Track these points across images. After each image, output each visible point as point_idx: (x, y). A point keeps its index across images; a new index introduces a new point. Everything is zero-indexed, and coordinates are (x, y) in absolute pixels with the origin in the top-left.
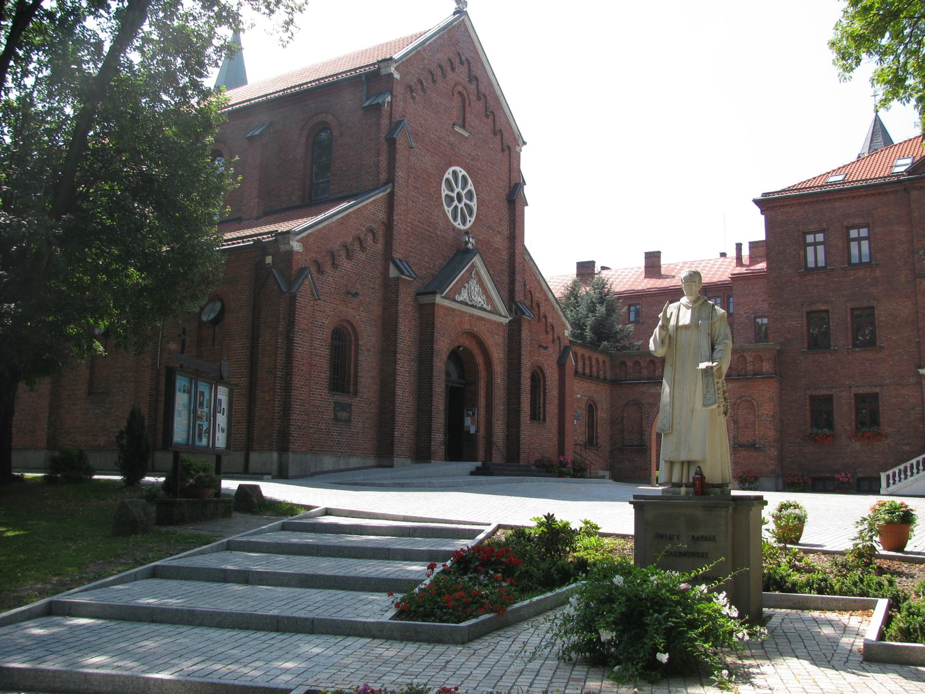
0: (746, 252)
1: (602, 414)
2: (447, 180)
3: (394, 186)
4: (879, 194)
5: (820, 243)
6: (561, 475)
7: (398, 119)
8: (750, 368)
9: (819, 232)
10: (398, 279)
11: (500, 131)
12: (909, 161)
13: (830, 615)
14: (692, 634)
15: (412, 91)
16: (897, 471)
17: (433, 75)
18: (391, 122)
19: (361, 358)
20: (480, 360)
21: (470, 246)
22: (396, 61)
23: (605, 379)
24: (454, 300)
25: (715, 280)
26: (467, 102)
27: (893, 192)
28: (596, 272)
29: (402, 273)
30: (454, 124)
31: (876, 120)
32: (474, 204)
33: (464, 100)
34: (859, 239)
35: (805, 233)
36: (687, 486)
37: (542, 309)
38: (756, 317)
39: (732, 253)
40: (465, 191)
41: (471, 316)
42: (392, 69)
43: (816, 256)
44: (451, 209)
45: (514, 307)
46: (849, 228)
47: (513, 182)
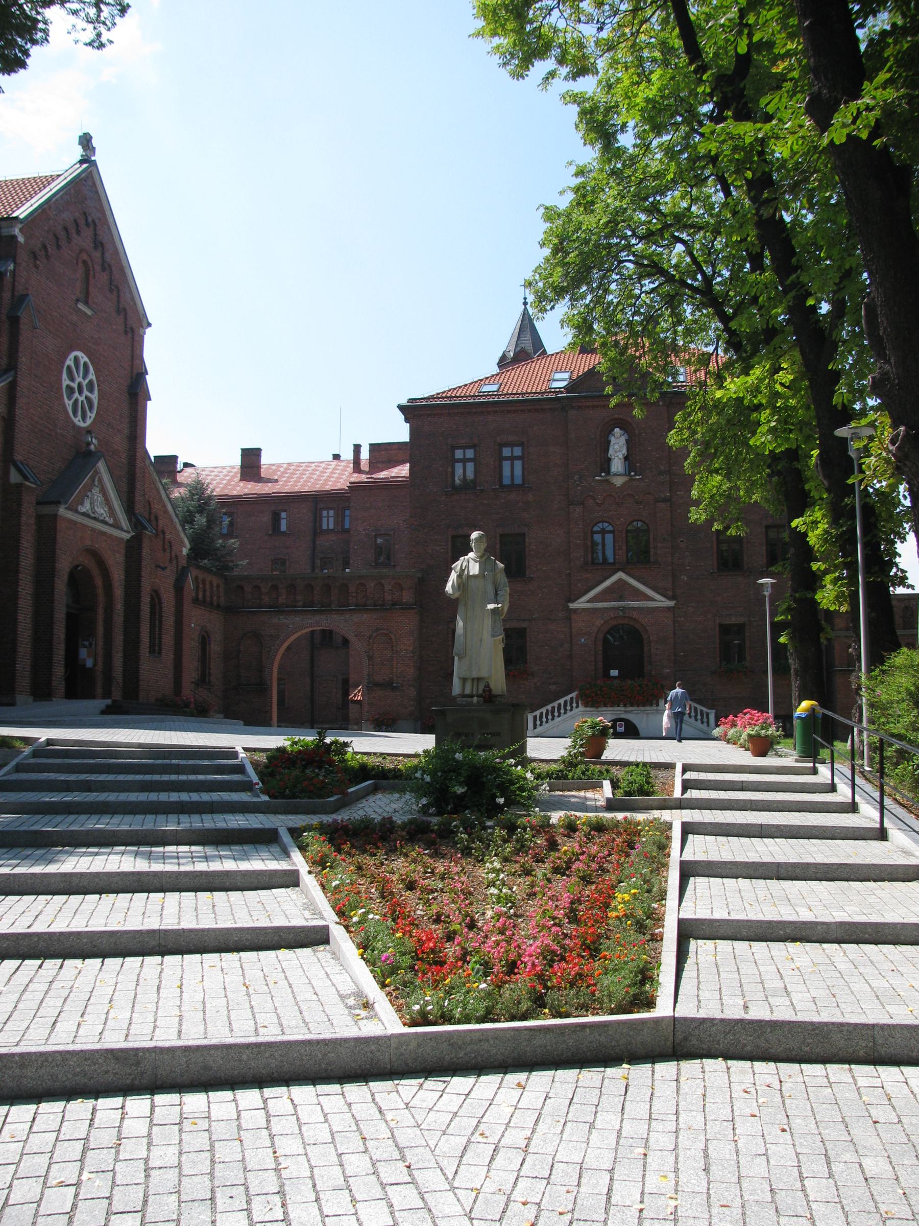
0: (365, 455)
1: (215, 648)
2: (69, 368)
3: (16, 373)
4: (536, 410)
5: (469, 460)
6: (185, 714)
8: (388, 597)
10: (19, 486)
11: (125, 309)
12: (566, 376)
14: (512, 788)
16: (544, 712)
17: (57, 239)
18: (13, 296)
20: (99, 582)
21: (92, 447)
23: (218, 606)
24: (77, 511)
25: (328, 488)
26: (92, 273)
27: (551, 409)
28: (179, 469)
29: (26, 478)
30: (78, 300)
31: (524, 314)
32: (95, 397)
33: (87, 271)
34: (512, 459)
35: (454, 448)
36: (478, 696)
37: (161, 523)
39: (348, 455)
40: (87, 381)
41: (93, 530)
42: (17, 231)
43: (463, 472)
44: (71, 402)
45: (134, 520)
47: (135, 372)
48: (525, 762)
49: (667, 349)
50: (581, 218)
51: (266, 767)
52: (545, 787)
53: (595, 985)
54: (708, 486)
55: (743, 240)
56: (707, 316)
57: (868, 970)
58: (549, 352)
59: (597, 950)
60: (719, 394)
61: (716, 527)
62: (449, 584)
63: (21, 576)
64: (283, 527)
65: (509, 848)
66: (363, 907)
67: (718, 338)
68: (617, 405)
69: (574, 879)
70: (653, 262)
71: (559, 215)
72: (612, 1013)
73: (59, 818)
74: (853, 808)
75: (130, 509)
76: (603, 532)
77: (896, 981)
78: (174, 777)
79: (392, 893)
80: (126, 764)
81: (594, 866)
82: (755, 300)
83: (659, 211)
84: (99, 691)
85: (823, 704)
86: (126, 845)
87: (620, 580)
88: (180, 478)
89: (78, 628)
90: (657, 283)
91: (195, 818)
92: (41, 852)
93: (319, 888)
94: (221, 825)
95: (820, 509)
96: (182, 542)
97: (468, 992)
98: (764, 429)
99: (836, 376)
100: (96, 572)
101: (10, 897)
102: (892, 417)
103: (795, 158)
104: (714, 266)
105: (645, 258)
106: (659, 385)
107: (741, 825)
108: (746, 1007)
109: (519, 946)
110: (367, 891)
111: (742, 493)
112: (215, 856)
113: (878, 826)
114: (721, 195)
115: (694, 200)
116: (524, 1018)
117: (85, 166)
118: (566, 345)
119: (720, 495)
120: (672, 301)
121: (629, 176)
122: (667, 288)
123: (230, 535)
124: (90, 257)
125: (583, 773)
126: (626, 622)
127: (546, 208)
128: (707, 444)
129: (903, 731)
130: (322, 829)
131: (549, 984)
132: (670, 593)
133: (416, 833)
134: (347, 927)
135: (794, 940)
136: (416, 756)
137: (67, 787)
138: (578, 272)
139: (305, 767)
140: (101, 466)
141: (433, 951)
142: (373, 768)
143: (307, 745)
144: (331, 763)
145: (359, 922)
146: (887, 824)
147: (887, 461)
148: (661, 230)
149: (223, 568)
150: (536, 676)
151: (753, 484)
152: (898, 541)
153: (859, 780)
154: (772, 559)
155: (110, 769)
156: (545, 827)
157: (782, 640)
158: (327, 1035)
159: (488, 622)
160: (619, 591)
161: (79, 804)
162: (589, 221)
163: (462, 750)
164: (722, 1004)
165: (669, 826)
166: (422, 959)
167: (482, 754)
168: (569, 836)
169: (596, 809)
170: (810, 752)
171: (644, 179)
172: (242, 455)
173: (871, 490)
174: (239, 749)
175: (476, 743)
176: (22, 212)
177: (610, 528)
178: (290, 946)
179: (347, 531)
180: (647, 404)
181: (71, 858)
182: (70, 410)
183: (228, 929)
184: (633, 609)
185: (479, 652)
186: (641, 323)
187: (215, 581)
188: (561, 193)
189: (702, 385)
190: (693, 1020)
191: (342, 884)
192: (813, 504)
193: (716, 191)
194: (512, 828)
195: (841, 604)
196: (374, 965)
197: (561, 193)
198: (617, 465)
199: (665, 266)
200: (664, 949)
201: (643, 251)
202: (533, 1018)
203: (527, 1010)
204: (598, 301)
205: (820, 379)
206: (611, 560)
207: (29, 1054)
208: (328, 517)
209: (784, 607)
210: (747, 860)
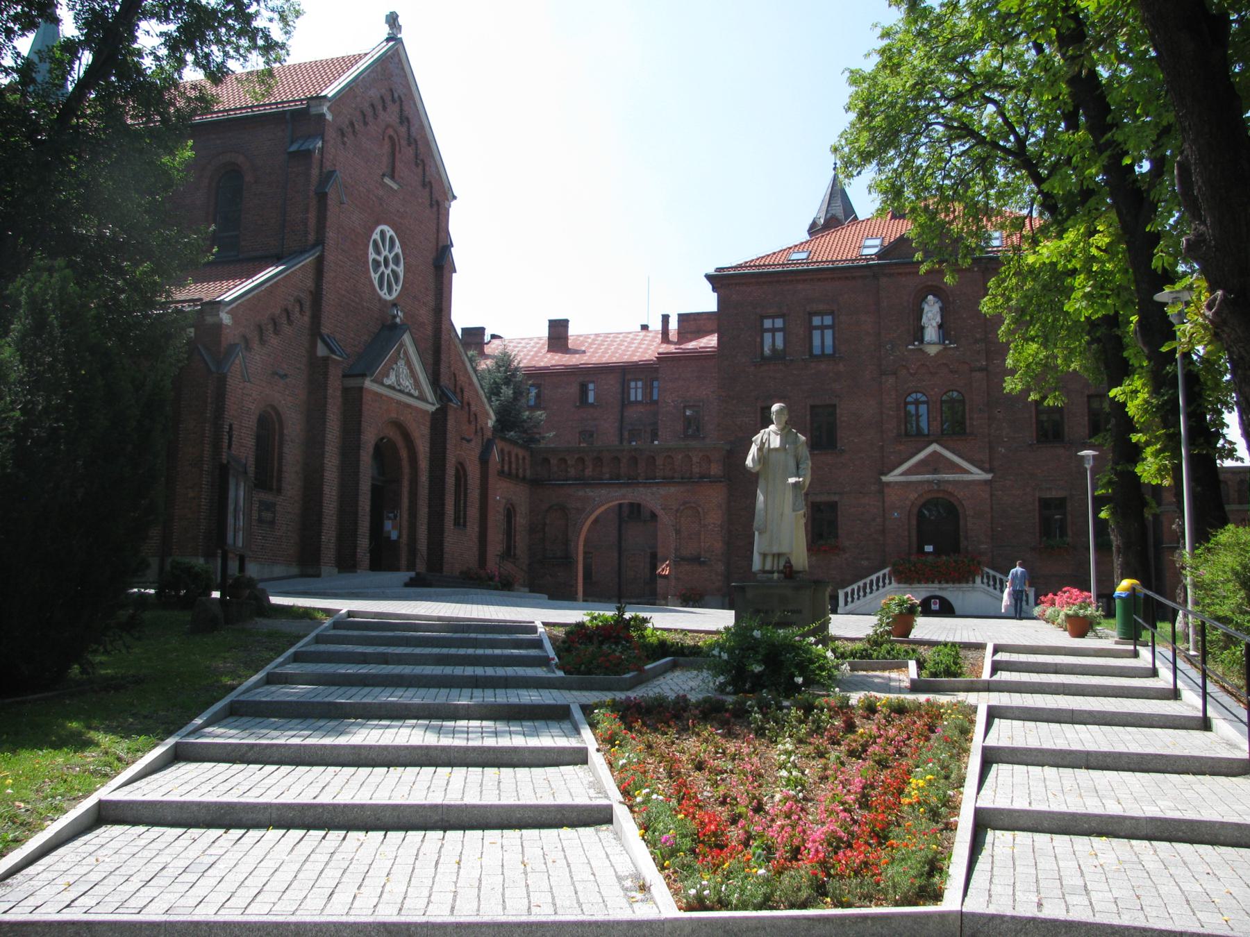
0: (673, 325)
1: (521, 520)
2: (375, 242)
4: (847, 278)
5: (779, 330)
6: (489, 587)
7: (329, 168)
8: (696, 470)
9: (778, 317)
10: (326, 359)
11: (430, 183)
12: (877, 242)
13: (878, 673)
14: (812, 667)
15: (343, 135)
17: (364, 116)
19: (286, 450)
20: (404, 454)
21: (398, 320)
22: (330, 100)
23: (524, 479)
24: (382, 384)
25: (635, 359)
30: (384, 175)
32: (400, 270)
33: (393, 146)
34: (822, 328)
35: (763, 317)
36: (779, 572)
38: (685, 407)
39: (656, 325)
41: (399, 402)
42: (325, 109)
43: (772, 342)
44: (377, 276)
46: (812, 314)
47: (441, 244)
48: (826, 640)
49: (978, 212)
50: (887, 81)
51: (564, 642)
52: (846, 667)
53: (880, 874)
54: (1023, 355)
55: (1055, 99)
56: (1020, 178)
57: (1180, 872)
58: (861, 218)
59: (886, 838)
60: (1031, 259)
61: (1033, 397)
62: (749, 458)
63: (327, 448)
64: (591, 399)
65: (804, 729)
66: (648, 787)
67: (1033, 200)
68: (928, 272)
69: (870, 763)
70: (963, 123)
71: (864, 79)
72: (897, 904)
73: (354, 690)
74: (1175, 694)
75: (435, 382)
76: (917, 403)
77: (1211, 885)
78: (470, 651)
79: (679, 773)
80: (423, 637)
81: (891, 749)
82: (1069, 161)
83: (968, 71)
84: (404, 562)
85: (1146, 583)
86: (418, 718)
87: (935, 452)
88: (488, 350)
89: (383, 499)
90: (967, 146)
91: (489, 692)
92: (333, 723)
93: (606, 767)
94: (514, 700)
95: (1140, 378)
96: (488, 414)
97: (746, 877)
98: (1078, 294)
99: (1156, 238)
100: (400, 443)
101: (300, 768)
102: (1208, 280)
103: (1101, 13)
104: (1027, 125)
105: (955, 120)
106: (970, 250)
107: (1051, 710)
108: (1040, 905)
109: (804, 832)
110: (656, 771)
111: (1059, 361)
112: (504, 732)
113: (1200, 714)
114: (1033, 52)
115: (1005, 59)
116: (803, 906)
117: (391, 43)
118: (873, 210)
119: (1037, 364)
120: (984, 164)
121: (937, 37)
122: (978, 150)
123: (537, 407)
124: (396, 131)
125: (888, 653)
126: (941, 495)
127: (852, 72)
128: (1021, 311)
129: (1229, 614)
130: (614, 706)
131: (832, 871)
132: (987, 466)
133: (711, 712)
134: (631, 808)
135: (1100, 834)
136: (717, 632)
137: (364, 659)
138: (885, 136)
139: (602, 643)
140: (407, 338)
141: (715, 834)
142: (673, 645)
143: (606, 620)
144: (629, 638)
145: (643, 802)
146: (1210, 713)
147: (1204, 327)
148: (970, 91)
149: (530, 441)
150: (841, 550)
151: (1072, 351)
152: (1225, 411)
153: (1181, 664)
154: (1095, 429)
155: (408, 642)
156: (844, 708)
157: (1103, 515)
158: (600, 917)
159: (789, 496)
160: (934, 463)
161: (375, 676)
162: (895, 84)
163: (760, 627)
164: (1014, 901)
165: (974, 709)
166: (703, 842)
167: (781, 631)
168: (868, 718)
169: (900, 690)
170: (1132, 634)
171: (952, 38)
173: (1195, 357)
174: (538, 624)
175: (776, 619)
176: (330, 91)
177: (924, 399)
178: (573, 825)
179: (656, 402)
180: (958, 270)
181: (363, 731)
182: (376, 283)
183: (511, 806)
184: (948, 482)
185: (781, 529)
186: (951, 187)
187: (521, 453)
188: (867, 56)
189: (1017, 249)
190: (982, 915)
191: (630, 763)
192: (1133, 373)
193: (1029, 48)
194: (808, 708)
195: (1163, 478)
196: (654, 846)
197: (867, 56)
198: (931, 334)
199: (976, 128)
200: (957, 839)
201: (953, 112)
202: (813, 907)
203: (807, 899)
204: (907, 165)
205: (1138, 241)
206: (926, 432)
207: (304, 923)
208: (636, 388)
209: (1105, 480)
210: (1054, 747)
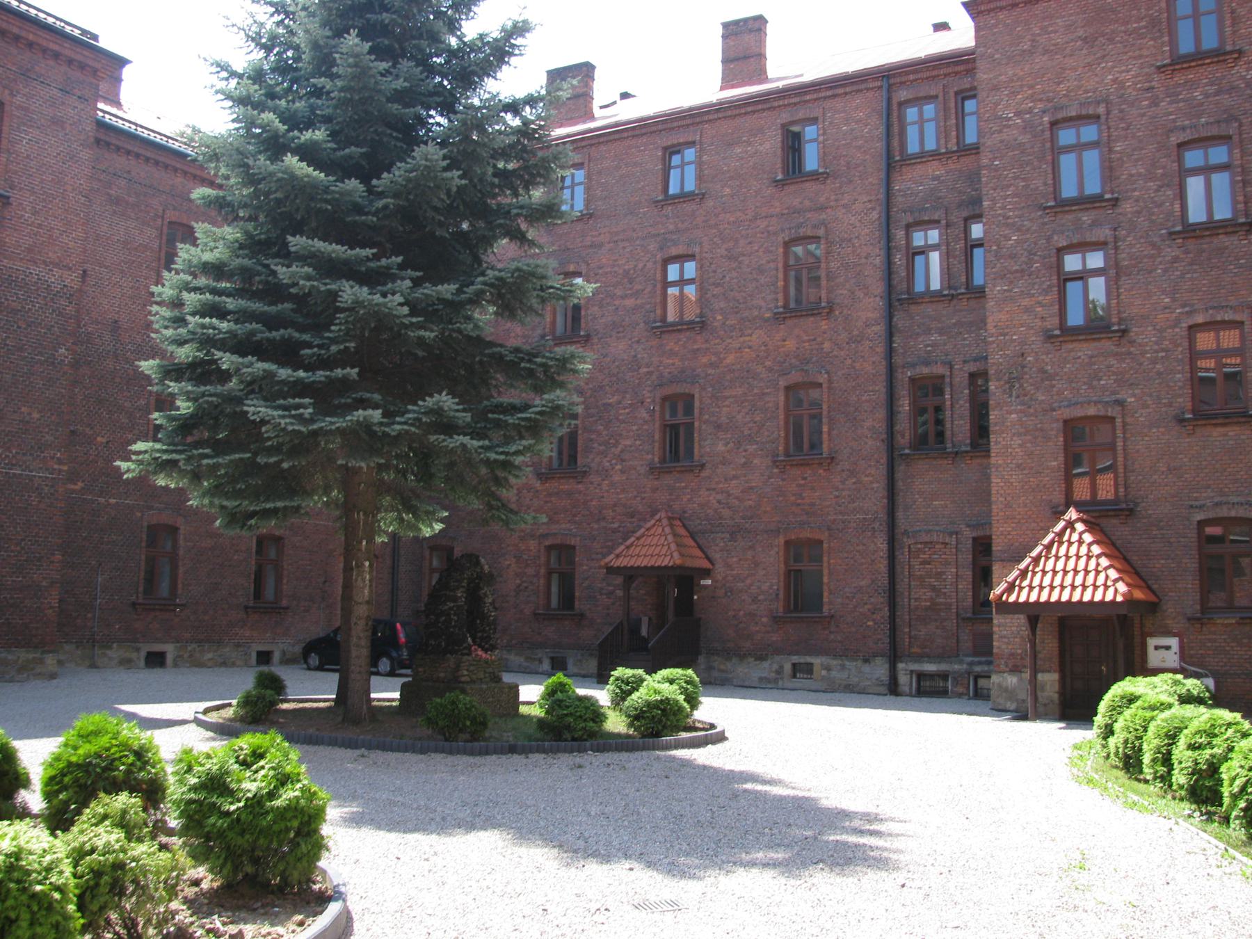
64: (811, 161)
172: (725, 37)
179: (975, 149)
208: (921, 122)
